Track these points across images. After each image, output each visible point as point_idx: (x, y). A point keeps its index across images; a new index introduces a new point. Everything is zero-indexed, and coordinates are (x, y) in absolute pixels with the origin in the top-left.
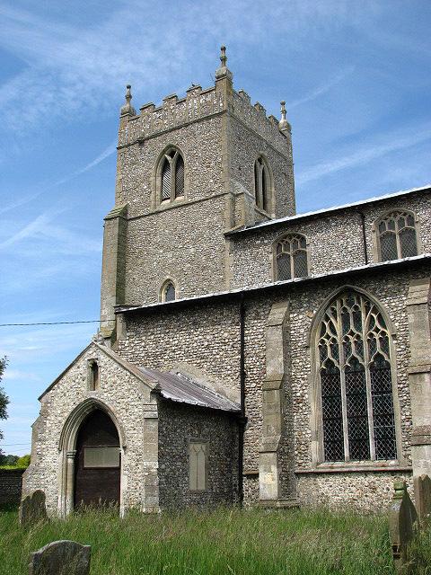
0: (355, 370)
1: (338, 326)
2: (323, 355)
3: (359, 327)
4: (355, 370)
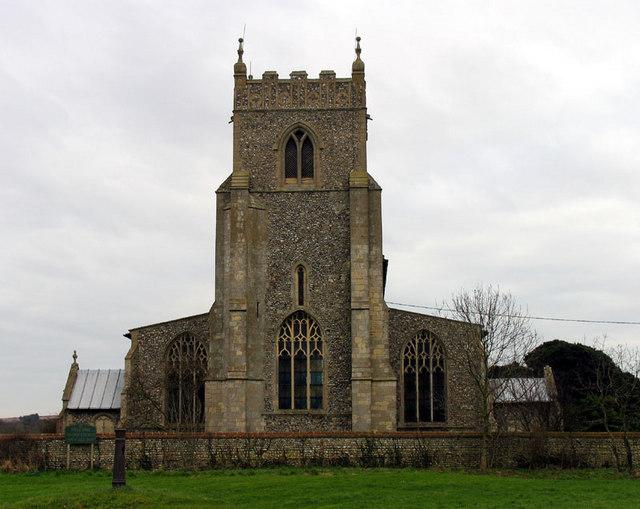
0: (424, 375)
1: (292, 331)
2: (281, 347)
3: (306, 335)
4: (424, 375)
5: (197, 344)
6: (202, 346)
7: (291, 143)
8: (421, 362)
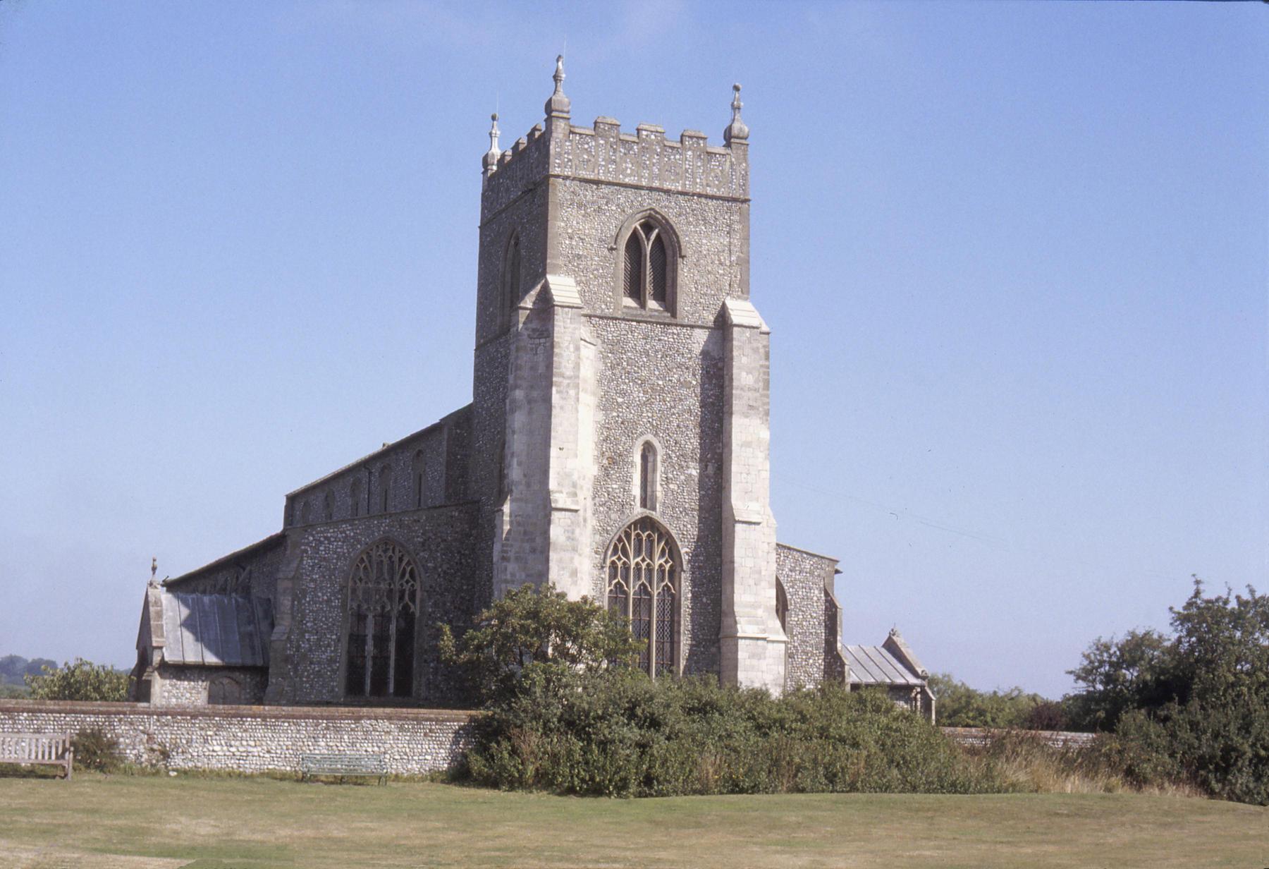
4: (384, 618)
5: (401, 560)
6: (408, 563)
7: (634, 244)
8: (402, 593)
